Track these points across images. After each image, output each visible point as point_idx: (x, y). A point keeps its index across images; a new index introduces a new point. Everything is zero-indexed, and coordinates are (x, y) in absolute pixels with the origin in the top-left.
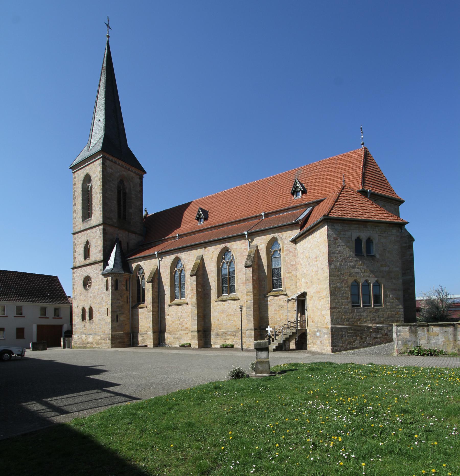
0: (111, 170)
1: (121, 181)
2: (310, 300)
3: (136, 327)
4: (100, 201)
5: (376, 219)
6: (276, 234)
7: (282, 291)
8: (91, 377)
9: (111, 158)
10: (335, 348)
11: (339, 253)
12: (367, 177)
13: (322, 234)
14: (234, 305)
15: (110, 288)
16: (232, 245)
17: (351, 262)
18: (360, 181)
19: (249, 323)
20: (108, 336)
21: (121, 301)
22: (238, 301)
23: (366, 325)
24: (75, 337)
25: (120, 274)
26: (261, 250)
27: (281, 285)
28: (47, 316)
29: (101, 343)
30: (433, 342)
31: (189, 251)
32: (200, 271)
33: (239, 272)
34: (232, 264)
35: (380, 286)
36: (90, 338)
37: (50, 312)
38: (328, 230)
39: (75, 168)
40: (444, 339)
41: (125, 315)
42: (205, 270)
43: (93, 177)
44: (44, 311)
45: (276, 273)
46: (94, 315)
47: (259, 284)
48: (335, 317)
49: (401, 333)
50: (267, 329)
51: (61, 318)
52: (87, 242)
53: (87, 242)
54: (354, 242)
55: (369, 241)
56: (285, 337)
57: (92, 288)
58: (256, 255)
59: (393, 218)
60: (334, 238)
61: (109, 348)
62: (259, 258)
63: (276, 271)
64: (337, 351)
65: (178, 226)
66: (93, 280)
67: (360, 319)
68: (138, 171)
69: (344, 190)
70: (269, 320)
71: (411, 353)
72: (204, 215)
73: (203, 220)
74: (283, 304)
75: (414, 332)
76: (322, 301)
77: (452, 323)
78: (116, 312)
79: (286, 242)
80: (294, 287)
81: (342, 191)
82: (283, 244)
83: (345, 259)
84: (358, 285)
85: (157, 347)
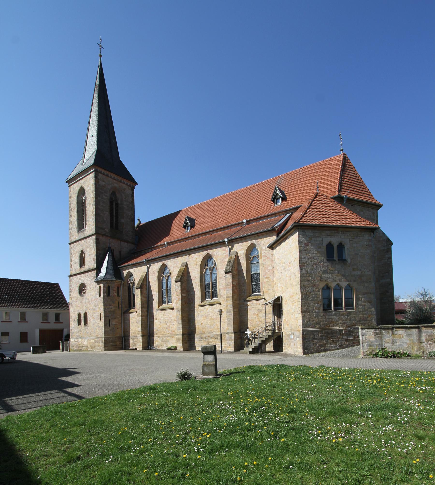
0: (103, 183)
1: (114, 193)
2: (285, 304)
3: (127, 331)
4: (93, 212)
5: (347, 225)
6: (254, 241)
7: (261, 295)
8: (62, 379)
9: (103, 171)
10: (307, 351)
11: (310, 258)
12: (345, 182)
13: (294, 241)
14: (216, 308)
15: (102, 294)
16: (214, 252)
17: (323, 267)
18: (337, 187)
19: (228, 327)
20: (101, 339)
21: (112, 307)
22: (219, 306)
23: (337, 327)
24: (72, 340)
25: (112, 281)
26: (241, 256)
27: (260, 289)
28: (49, 321)
29: (95, 347)
30: (398, 344)
31: (175, 258)
32: (184, 277)
33: (221, 278)
34: (214, 270)
35: (352, 289)
36: (86, 341)
37: (52, 318)
38: (299, 237)
39: (70, 181)
40: (408, 342)
41: (116, 320)
42: (189, 276)
43: (86, 189)
44: (45, 315)
45: (255, 278)
46: (88, 320)
47: (239, 289)
48: (306, 320)
49: (367, 335)
50: (246, 332)
51: (62, 323)
52: (82, 252)
53: (82, 252)
54: (325, 248)
55: (341, 246)
56: (261, 340)
57: (86, 294)
58: (236, 261)
59: (365, 223)
60: (305, 244)
61: (102, 350)
62: (239, 264)
63: (255, 276)
64: (308, 353)
65: (167, 234)
66: (88, 287)
67: (331, 322)
68: (129, 183)
69: (318, 197)
70: (249, 323)
71: (376, 355)
72: (191, 223)
73: (190, 228)
74: (261, 308)
75: (379, 335)
76: (295, 305)
77: (417, 325)
78: (108, 317)
79: (264, 248)
80: (271, 291)
81: (315, 198)
82: (262, 250)
83: (316, 264)
84: (341, 289)
85: (146, 349)
